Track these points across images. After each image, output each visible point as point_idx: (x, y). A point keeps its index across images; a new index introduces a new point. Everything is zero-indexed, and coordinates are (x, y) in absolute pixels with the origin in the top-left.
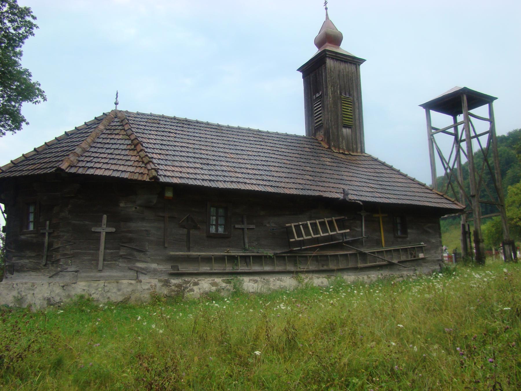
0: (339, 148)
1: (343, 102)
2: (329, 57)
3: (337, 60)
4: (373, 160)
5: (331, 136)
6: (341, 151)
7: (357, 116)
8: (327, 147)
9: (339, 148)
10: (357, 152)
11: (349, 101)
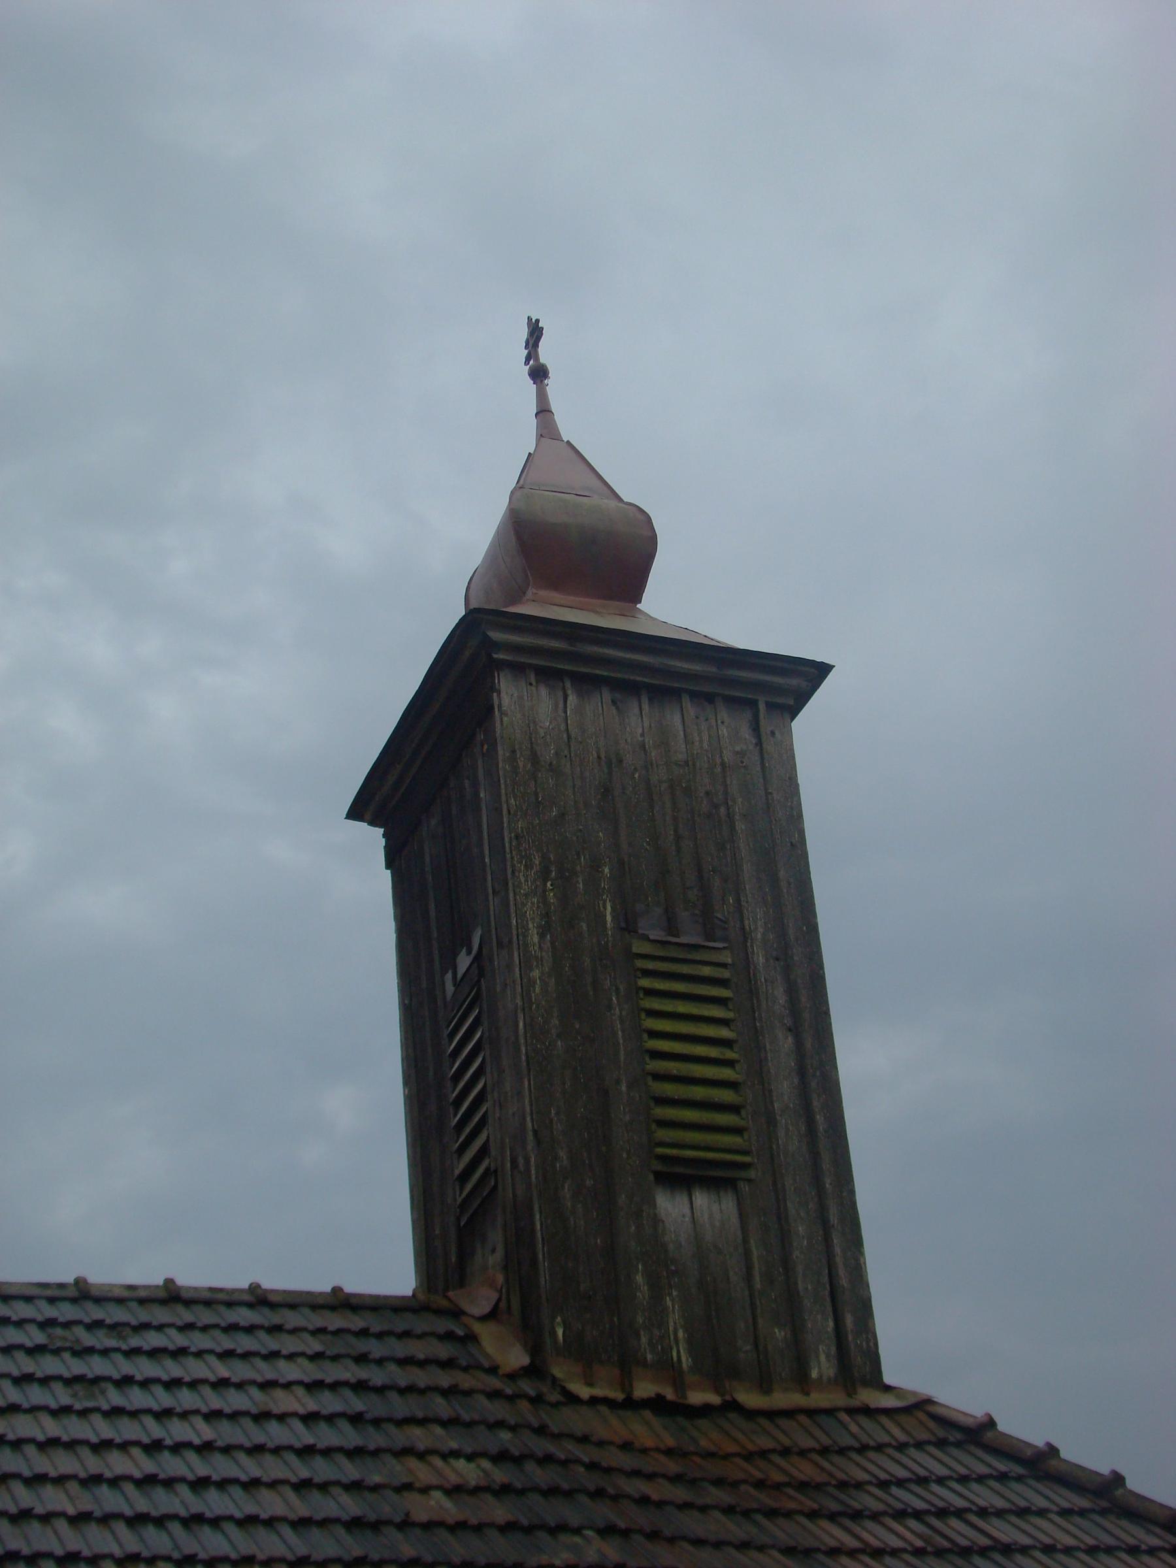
0: (627, 1365)
1: (645, 983)
2: (518, 669)
3: (587, 683)
4: (941, 1444)
5: (544, 1265)
6: (644, 1389)
7: (784, 1089)
8: (516, 1358)
9: (627, 1365)
10: (802, 1381)
11: (706, 971)
